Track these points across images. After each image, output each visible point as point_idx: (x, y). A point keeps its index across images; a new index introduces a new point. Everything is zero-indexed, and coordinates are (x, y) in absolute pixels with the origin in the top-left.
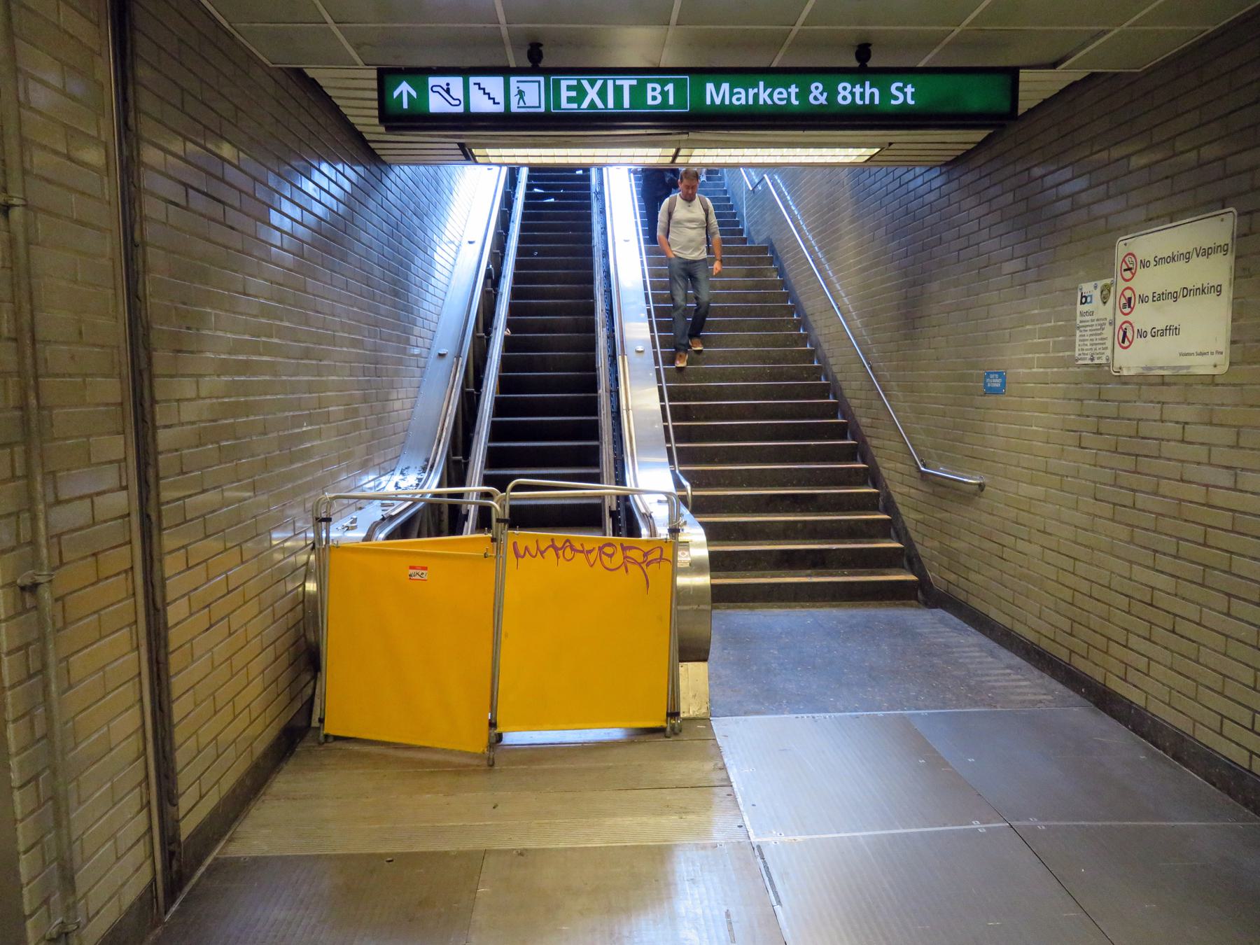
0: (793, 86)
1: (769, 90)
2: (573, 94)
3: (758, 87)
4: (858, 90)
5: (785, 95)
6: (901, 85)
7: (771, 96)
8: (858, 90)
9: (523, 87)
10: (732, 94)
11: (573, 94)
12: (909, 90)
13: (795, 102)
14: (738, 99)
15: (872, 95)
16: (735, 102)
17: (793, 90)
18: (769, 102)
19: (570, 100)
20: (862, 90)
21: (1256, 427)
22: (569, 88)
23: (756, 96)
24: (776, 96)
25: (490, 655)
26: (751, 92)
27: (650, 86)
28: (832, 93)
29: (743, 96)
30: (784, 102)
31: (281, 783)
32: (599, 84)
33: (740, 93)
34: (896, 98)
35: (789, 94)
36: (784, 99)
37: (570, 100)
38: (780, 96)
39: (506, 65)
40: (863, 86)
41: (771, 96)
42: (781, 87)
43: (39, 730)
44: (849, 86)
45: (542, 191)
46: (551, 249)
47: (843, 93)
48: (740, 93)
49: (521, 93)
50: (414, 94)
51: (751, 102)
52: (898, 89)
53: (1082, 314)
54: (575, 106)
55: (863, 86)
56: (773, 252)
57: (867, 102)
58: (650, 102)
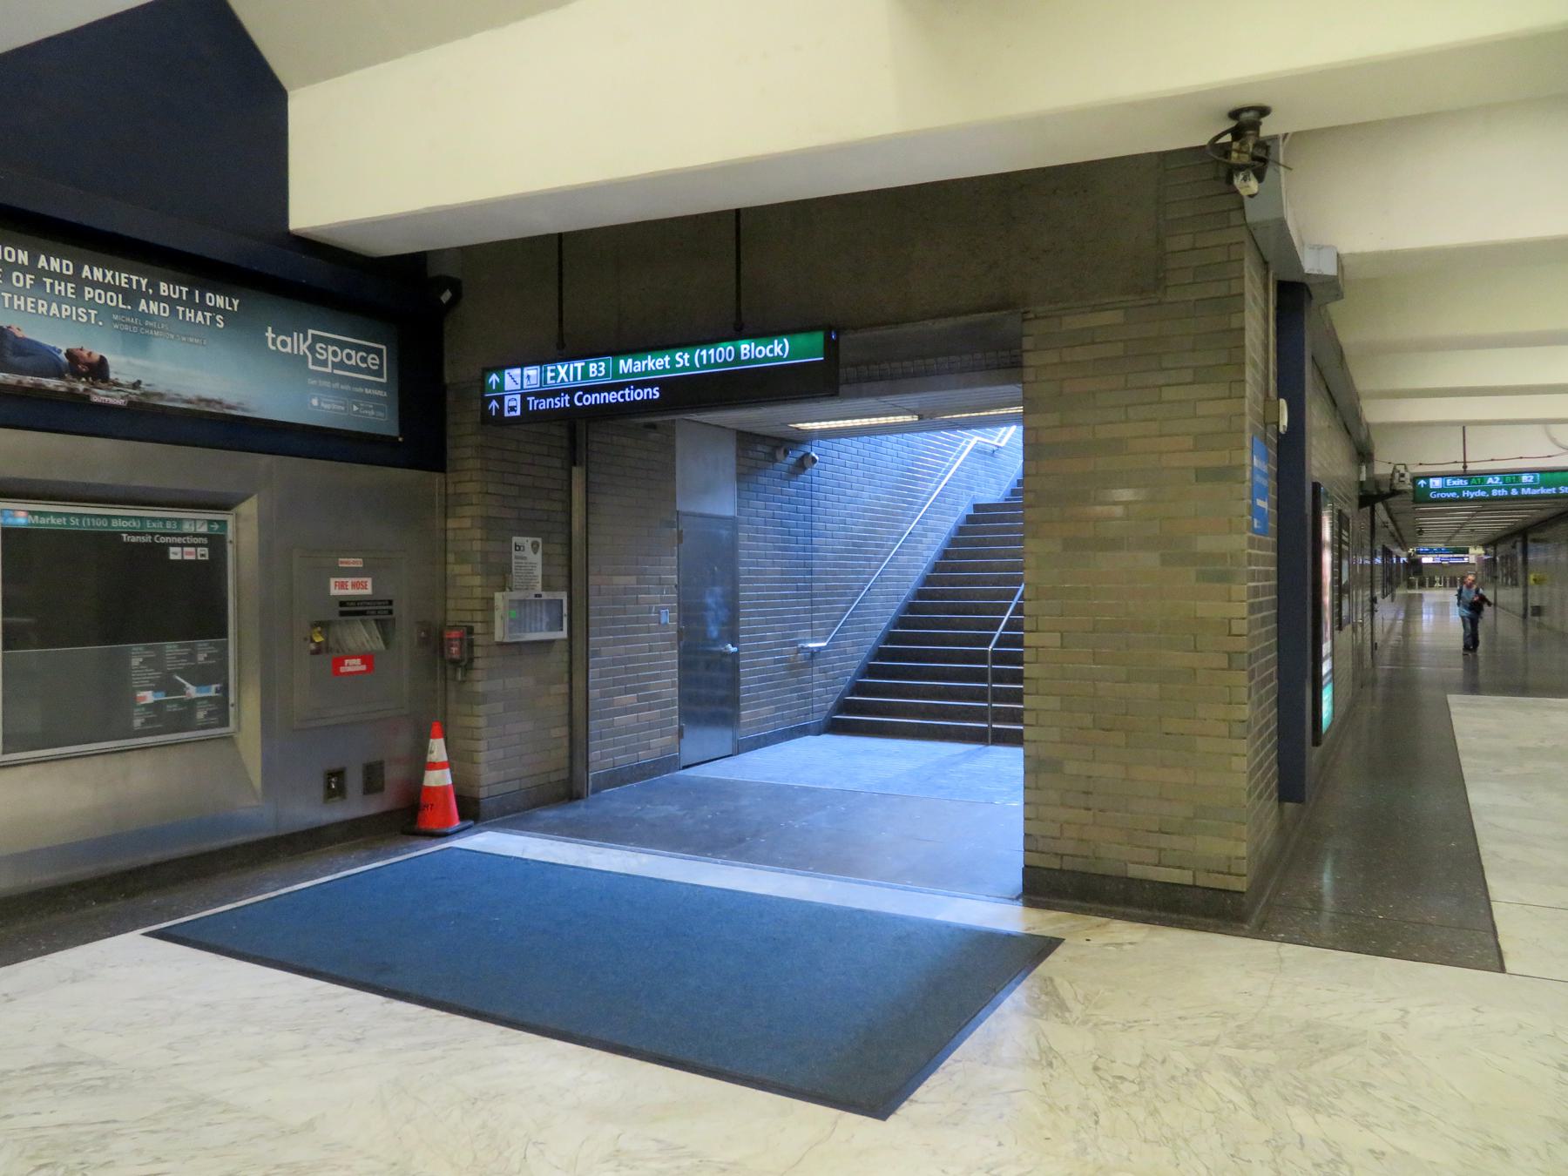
0: (667, 356)
1: (654, 361)
3: (773, 344)
6: (681, 354)
7: (654, 364)
10: (633, 365)
16: (635, 371)
17: (667, 358)
18: (654, 368)
21: (1566, 1043)
23: (646, 365)
24: (657, 364)
26: (644, 363)
27: (591, 365)
32: (566, 366)
34: (679, 363)
41: (654, 364)
45: (800, 425)
50: (498, 380)
52: (680, 357)
53: (516, 557)
54: (554, 382)
58: (591, 375)
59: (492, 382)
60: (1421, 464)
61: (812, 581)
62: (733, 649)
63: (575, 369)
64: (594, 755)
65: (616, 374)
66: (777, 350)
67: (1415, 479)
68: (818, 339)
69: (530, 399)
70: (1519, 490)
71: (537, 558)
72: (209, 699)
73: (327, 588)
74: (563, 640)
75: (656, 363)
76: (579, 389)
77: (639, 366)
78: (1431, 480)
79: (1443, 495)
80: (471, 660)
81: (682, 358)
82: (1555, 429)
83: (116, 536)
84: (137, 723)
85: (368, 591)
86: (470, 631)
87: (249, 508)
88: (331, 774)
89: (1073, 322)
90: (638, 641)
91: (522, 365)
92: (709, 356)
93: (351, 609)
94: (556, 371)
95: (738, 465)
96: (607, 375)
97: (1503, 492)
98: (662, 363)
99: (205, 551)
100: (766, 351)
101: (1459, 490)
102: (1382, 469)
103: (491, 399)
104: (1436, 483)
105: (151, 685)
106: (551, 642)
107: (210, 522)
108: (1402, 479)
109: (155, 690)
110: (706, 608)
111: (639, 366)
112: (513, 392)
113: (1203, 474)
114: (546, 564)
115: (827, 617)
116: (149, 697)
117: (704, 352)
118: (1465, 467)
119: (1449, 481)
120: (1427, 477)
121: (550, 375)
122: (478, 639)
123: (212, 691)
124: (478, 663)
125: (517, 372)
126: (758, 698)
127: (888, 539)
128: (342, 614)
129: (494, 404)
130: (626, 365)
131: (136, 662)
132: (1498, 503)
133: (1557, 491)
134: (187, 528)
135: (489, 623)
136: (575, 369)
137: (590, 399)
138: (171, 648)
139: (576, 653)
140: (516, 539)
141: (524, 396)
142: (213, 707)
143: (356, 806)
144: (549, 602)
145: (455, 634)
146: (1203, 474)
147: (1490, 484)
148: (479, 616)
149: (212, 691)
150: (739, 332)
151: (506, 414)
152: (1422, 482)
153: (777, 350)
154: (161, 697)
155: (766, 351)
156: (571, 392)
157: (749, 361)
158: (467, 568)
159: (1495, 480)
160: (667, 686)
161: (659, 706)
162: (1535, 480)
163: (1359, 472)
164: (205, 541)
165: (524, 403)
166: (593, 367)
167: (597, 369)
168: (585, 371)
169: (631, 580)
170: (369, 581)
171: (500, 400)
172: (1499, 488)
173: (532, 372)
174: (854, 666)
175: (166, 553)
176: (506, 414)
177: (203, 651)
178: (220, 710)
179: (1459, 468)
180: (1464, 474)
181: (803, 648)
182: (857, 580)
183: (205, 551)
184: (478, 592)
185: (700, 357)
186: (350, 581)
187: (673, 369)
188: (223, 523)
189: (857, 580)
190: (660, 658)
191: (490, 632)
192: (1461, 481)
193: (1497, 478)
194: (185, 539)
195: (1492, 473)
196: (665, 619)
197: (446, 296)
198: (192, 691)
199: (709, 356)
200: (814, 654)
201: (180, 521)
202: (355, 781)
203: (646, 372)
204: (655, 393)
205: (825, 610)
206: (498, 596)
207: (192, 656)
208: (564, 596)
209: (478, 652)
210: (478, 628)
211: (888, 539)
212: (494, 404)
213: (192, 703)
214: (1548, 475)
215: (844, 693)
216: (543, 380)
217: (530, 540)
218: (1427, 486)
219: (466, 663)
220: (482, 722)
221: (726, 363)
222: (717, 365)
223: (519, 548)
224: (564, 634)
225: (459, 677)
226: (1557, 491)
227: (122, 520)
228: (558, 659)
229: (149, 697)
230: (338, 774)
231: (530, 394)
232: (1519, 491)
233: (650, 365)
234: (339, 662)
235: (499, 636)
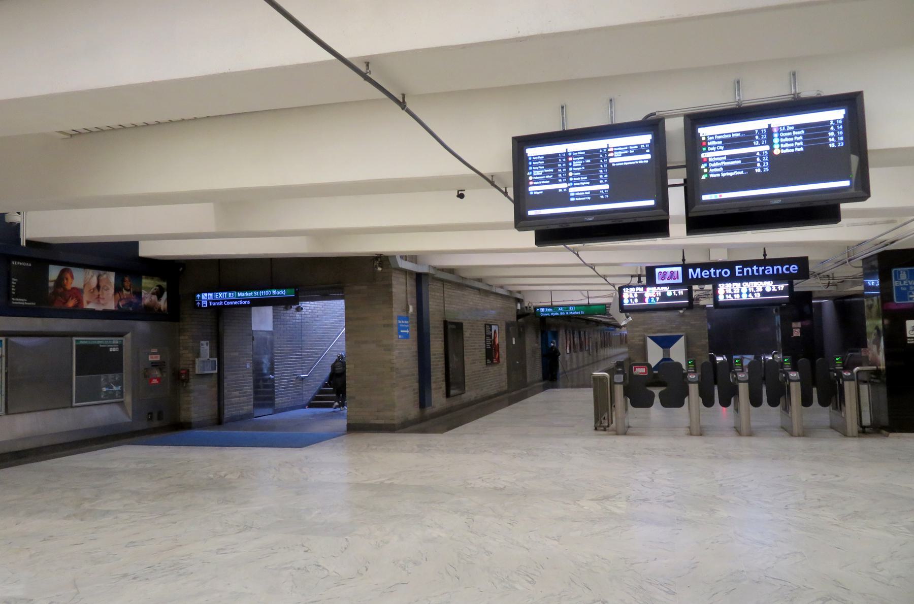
2: (741, 271)
5: (708, 273)
11: (741, 271)
14: (768, 272)
19: (739, 273)
20: (757, 268)
22: (739, 269)
24: (791, 269)
25: (456, 159)
28: (254, 294)
29: (771, 270)
30: (708, 277)
31: (216, 409)
33: (769, 269)
35: (710, 273)
36: (707, 275)
37: (739, 273)
38: (794, 269)
42: (797, 265)
43: (598, 520)
48: (769, 269)
51: (775, 272)
56: (496, 364)
61: (302, 352)
62: (273, 377)
63: (224, 294)
64: (226, 411)
65: (237, 296)
66: (282, 293)
67: (535, 309)
68: (293, 291)
69: (210, 302)
70: (569, 312)
71: (208, 348)
72: (119, 390)
73: (148, 358)
74: (215, 373)
75: (248, 294)
76: (225, 300)
77: (244, 295)
78: (541, 309)
80: (189, 380)
81: (256, 293)
82: (583, 292)
83: (98, 345)
84: (102, 396)
85: (159, 359)
86: (188, 371)
87: (129, 335)
88: (149, 414)
89: (356, 288)
90: (239, 374)
91: (207, 292)
92: (264, 293)
93: (155, 365)
94: (219, 295)
95: (273, 312)
96: (234, 297)
97: (564, 313)
99: (117, 348)
100: (279, 293)
101: (550, 313)
102: (526, 305)
103: (197, 302)
104: (542, 310)
106: (212, 374)
107: (119, 340)
109: (106, 387)
110: (263, 363)
111: (244, 295)
112: (204, 300)
113: (384, 326)
114: (210, 349)
115: (309, 366)
116: (104, 389)
117: (262, 292)
118: (552, 304)
120: (540, 307)
121: (216, 296)
122: (191, 373)
123: (119, 388)
124: (191, 380)
125: (206, 295)
126: (282, 394)
127: (333, 336)
128: (153, 366)
129: (198, 303)
130: (240, 294)
131: (102, 379)
134: (114, 342)
135: (194, 368)
136: (224, 294)
137: (229, 303)
138: (110, 376)
139: (220, 377)
140: (202, 342)
141: (208, 302)
142: (120, 393)
143: (156, 423)
144: (212, 361)
145: (184, 372)
146: (384, 326)
148: (191, 366)
149: (119, 388)
150: (271, 288)
151: (203, 306)
152: (538, 310)
153: (282, 293)
154: (107, 389)
155: (279, 293)
156: (223, 301)
157: (275, 295)
158: (187, 351)
160: (249, 389)
161: (247, 396)
163: (517, 306)
164: (117, 346)
165: (208, 303)
166: (230, 294)
167: (231, 295)
168: (227, 295)
169: (236, 354)
170: (159, 356)
171: (201, 302)
172: (562, 312)
173: (211, 295)
174: (320, 384)
175: (109, 350)
176: (203, 306)
177: (117, 377)
178: (121, 393)
179: (550, 304)
180: (552, 307)
181: (298, 377)
182: (320, 352)
183: (117, 348)
184: (191, 359)
185: (261, 293)
186: (154, 356)
187: (254, 296)
188: (122, 341)
189: (320, 352)
190: (247, 379)
191: (194, 371)
194: (113, 345)
195: (560, 306)
196: (248, 366)
197: (181, 269)
198: (115, 388)
199: (264, 293)
200: (303, 379)
201: (112, 340)
202: (155, 415)
203: (246, 297)
204: (248, 302)
205: (307, 363)
206: (197, 360)
207: (115, 378)
208: (216, 359)
209: (191, 377)
210: (191, 370)
211: (333, 336)
212: (198, 303)
213: (115, 391)
215: (316, 394)
216: (214, 297)
217: (206, 342)
219: (187, 381)
220: (192, 398)
221: (268, 295)
222: (266, 296)
223: (202, 345)
224: (216, 371)
225: (185, 385)
227: (99, 341)
228: (215, 379)
229: (104, 389)
230: (151, 413)
231: (210, 301)
233: (247, 295)
234: (151, 380)
235: (197, 372)
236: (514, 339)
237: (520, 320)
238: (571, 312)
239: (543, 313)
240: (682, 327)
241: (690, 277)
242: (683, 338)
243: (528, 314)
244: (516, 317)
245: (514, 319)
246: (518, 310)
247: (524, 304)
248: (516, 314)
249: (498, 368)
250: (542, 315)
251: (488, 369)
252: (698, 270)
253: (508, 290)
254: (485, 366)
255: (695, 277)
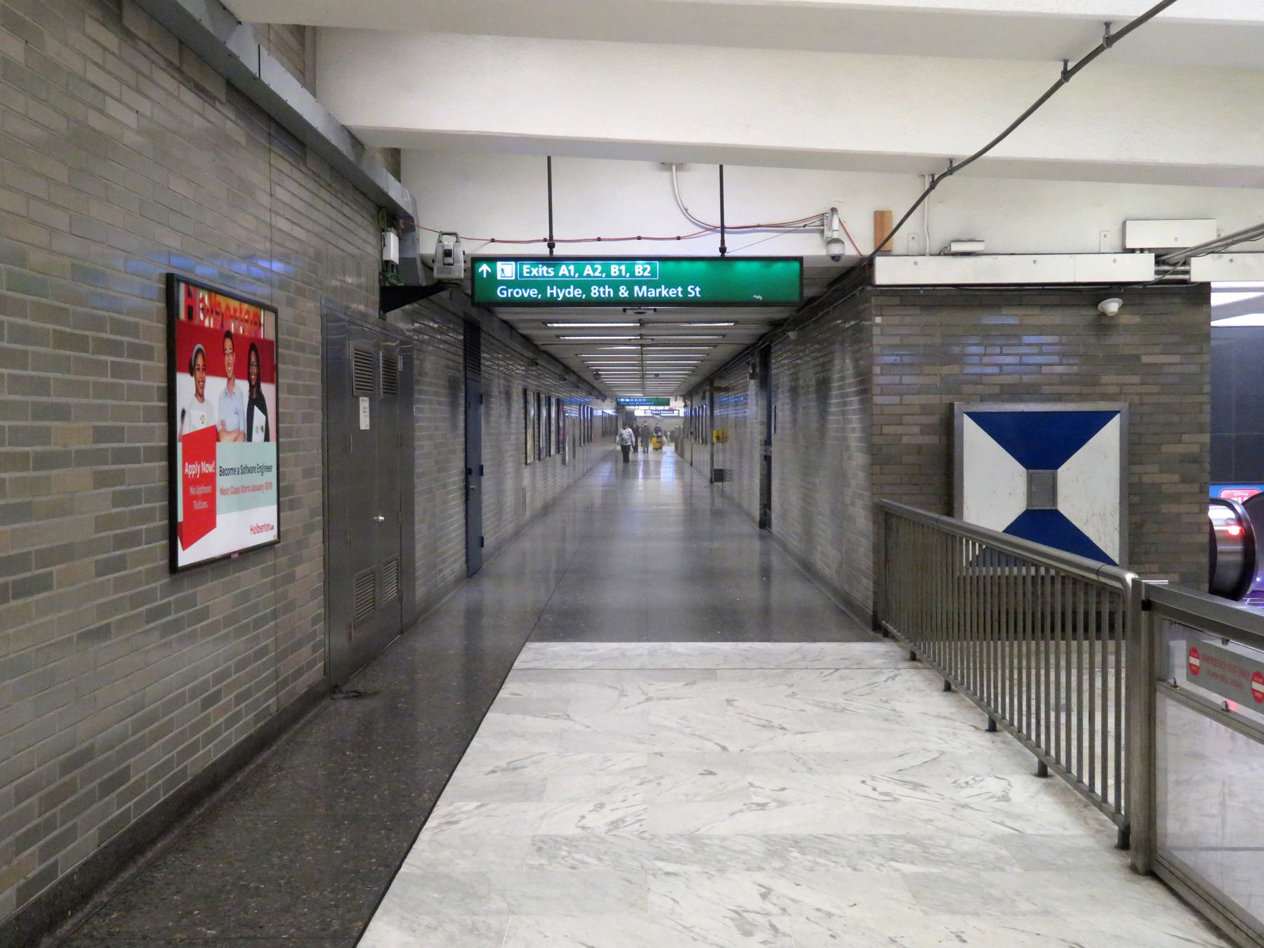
4: (602, 289)
7: (668, 292)
8: (602, 289)
9: (504, 267)
10: (648, 292)
12: (698, 289)
13: (680, 295)
15: (609, 292)
16: (649, 295)
23: (660, 292)
24: (671, 293)
26: (658, 290)
29: (654, 292)
34: (691, 294)
39: (222, 40)
40: (604, 288)
41: (668, 292)
44: (597, 288)
46: (695, 350)
47: (594, 291)
49: (502, 270)
50: (490, 270)
55: (604, 288)
57: (607, 295)
59: (482, 271)
60: (493, 241)
67: (476, 260)
78: (499, 265)
79: (519, 293)
98: (675, 292)
102: (428, 246)
104: (506, 271)
105: (1174, 509)
108: (450, 260)
119: (526, 267)
120: (492, 260)
132: (527, 309)
133: (685, 292)
147: (588, 275)
152: (484, 268)
159: (594, 270)
162: (653, 273)
163: (383, 244)
172: (601, 284)
179: (543, 250)
192: (545, 268)
193: (599, 267)
214: (671, 265)
218: (492, 275)
226: (685, 292)
232: (631, 291)
236: (364, 404)
237: (394, 316)
238: (640, 284)
239: (509, 284)
240: (1105, 379)
241: (636, 295)
242: (1115, 423)
243: (440, 285)
244: (376, 297)
245: (366, 305)
246: (387, 265)
247: (415, 242)
248: (377, 285)
249: (265, 573)
250: (502, 293)
251: (190, 601)
252: (644, 288)
253: (315, 96)
254: (165, 580)
255: (640, 295)
